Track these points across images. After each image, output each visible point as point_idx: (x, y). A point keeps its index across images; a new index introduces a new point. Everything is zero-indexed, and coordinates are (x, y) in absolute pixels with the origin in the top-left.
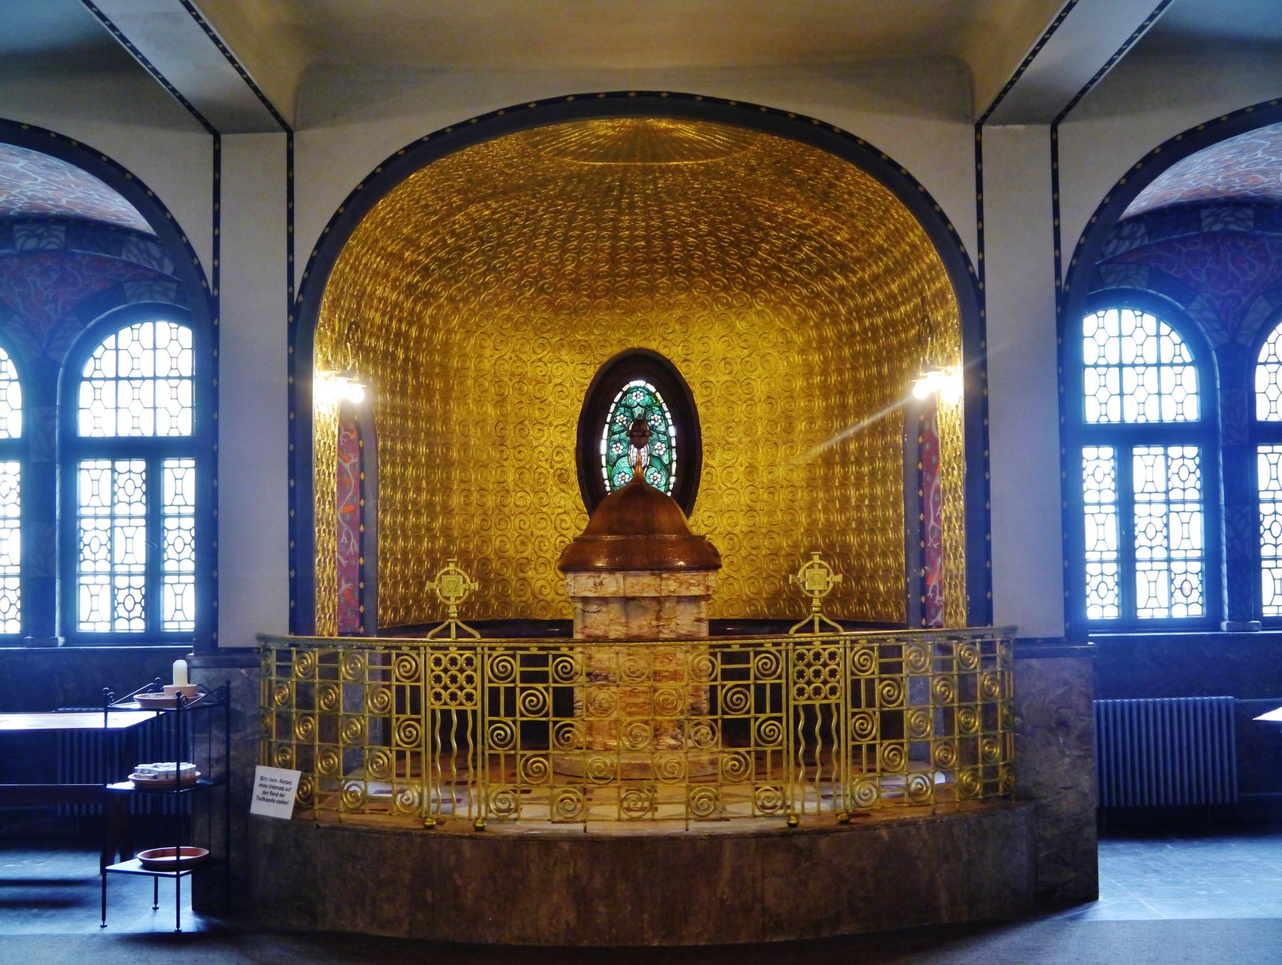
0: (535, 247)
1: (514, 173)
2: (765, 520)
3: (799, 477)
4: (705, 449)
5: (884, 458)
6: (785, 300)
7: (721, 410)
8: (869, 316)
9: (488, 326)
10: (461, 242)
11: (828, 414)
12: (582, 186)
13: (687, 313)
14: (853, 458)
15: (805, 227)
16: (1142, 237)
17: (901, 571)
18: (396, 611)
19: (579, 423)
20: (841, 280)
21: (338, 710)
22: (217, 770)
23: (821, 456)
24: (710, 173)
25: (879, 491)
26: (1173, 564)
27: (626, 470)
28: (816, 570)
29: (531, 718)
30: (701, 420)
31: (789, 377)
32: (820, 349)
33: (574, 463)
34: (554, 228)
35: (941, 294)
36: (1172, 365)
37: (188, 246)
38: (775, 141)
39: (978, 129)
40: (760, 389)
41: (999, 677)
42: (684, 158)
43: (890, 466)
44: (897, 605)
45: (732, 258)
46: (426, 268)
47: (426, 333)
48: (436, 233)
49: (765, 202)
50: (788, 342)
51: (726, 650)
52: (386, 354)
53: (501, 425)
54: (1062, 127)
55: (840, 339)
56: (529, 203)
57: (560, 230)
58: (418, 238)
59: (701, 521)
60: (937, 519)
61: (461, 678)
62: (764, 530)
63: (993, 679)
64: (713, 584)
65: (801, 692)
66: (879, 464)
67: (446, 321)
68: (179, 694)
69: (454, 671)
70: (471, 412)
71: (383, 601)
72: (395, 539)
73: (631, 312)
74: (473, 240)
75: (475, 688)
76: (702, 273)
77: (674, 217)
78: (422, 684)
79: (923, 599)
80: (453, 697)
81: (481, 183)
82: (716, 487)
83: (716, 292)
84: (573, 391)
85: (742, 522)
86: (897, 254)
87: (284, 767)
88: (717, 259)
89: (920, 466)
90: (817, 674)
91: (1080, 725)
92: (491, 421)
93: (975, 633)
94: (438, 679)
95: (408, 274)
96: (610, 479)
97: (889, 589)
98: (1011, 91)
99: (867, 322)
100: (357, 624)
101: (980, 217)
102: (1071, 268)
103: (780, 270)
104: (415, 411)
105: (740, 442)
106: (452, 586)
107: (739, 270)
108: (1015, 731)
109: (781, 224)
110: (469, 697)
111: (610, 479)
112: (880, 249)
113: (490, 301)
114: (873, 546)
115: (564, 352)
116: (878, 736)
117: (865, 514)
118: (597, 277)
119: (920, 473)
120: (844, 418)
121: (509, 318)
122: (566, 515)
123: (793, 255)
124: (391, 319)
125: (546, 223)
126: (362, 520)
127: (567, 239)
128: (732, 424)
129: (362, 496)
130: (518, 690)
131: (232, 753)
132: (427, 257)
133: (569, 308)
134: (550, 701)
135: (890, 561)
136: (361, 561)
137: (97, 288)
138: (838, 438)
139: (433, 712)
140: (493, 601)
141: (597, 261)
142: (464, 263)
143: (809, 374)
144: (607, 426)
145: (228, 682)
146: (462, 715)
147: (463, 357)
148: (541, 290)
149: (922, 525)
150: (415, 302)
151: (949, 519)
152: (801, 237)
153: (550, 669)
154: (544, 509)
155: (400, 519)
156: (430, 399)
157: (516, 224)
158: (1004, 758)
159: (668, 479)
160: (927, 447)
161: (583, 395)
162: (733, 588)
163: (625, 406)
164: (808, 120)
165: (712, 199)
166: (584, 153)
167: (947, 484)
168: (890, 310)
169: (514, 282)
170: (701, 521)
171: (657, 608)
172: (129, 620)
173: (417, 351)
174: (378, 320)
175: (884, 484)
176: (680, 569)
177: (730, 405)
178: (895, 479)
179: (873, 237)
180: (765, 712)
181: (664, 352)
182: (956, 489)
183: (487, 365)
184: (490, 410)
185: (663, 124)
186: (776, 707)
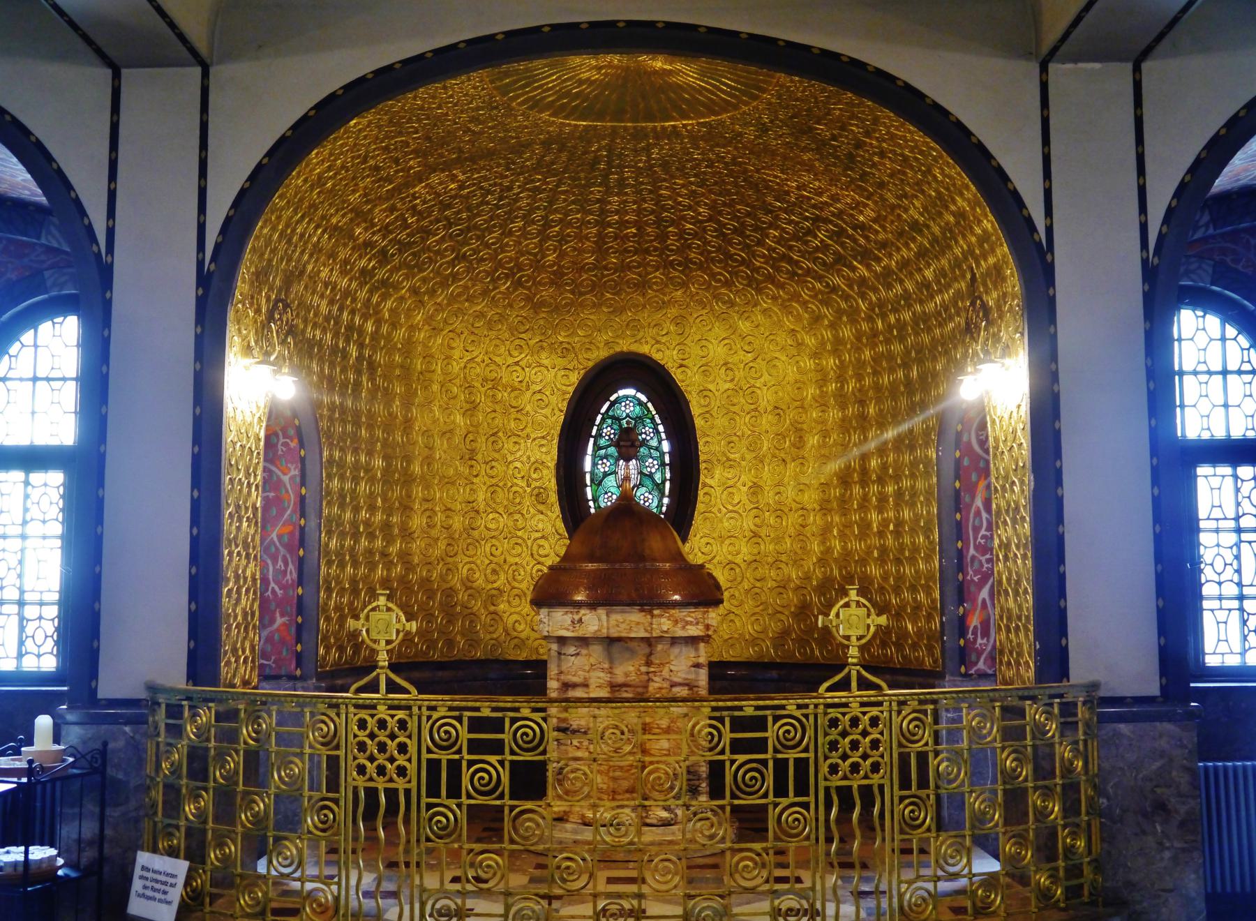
0: (511, 233)
1: (481, 133)
2: (771, 547)
3: (811, 498)
4: (702, 466)
5: (913, 476)
6: (796, 297)
7: (721, 422)
8: (895, 310)
9: (457, 324)
10: (425, 223)
11: (845, 426)
12: (564, 156)
13: (683, 312)
14: (874, 477)
15: (821, 207)
16: (1207, 225)
17: (935, 608)
18: (341, 649)
19: (561, 436)
20: (863, 271)
21: (237, 784)
22: (89, 855)
23: (836, 474)
24: (712, 136)
25: (906, 514)
26: (1245, 602)
27: (613, 490)
28: (853, 609)
29: (481, 800)
30: (698, 433)
31: (799, 385)
32: (836, 352)
33: (554, 481)
34: (532, 210)
35: (997, 271)
36: (1240, 372)
37: (78, 203)
38: (794, 83)
39: (1044, 68)
40: (766, 398)
41: (1081, 747)
42: (685, 116)
43: (920, 485)
44: (930, 649)
45: (735, 241)
46: (383, 252)
47: (385, 329)
48: (392, 209)
49: (774, 176)
50: (799, 344)
51: (737, 713)
52: (334, 350)
53: (471, 437)
54: (1145, 66)
55: (859, 339)
56: (503, 177)
57: (539, 213)
58: (370, 211)
59: (699, 547)
60: (985, 549)
61: (392, 746)
62: (770, 560)
63: (1075, 750)
64: (713, 623)
65: (834, 769)
66: (906, 483)
67: (408, 317)
68: (30, 762)
69: (382, 737)
70: (437, 418)
71: (325, 638)
72: (342, 565)
73: (620, 311)
74: (438, 221)
75: (409, 760)
76: (700, 267)
77: (670, 198)
78: (341, 753)
79: (962, 642)
80: (381, 771)
81: (443, 143)
82: (715, 510)
83: (716, 288)
84: (553, 399)
85: (744, 550)
86: (936, 230)
87: (170, 855)
88: (719, 249)
89: (957, 484)
90: (855, 745)
91: (1183, 809)
92: (460, 433)
93: (1053, 692)
94: (362, 747)
95: (360, 257)
96: (595, 500)
97: (919, 629)
98: (1073, 36)
99: (892, 319)
100: (293, 666)
101: (1047, 174)
102: (1161, 237)
103: (790, 261)
104: (371, 416)
105: (743, 459)
106: (381, 626)
107: (743, 262)
108: (1101, 817)
109: (794, 204)
110: (402, 771)
111: (595, 500)
112: (915, 226)
113: (459, 295)
114: (900, 578)
115: (544, 355)
116: (933, 827)
117: (890, 541)
118: (582, 269)
119: (957, 493)
120: (864, 430)
121: (481, 315)
122: (544, 537)
123: (806, 243)
124: (341, 309)
125: (523, 203)
126: (302, 543)
127: (547, 225)
128: (735, 438)
129: (303, 515)
130: (464, 764)
131: (108, 832)
132: (384, 238)
133: (550, 305)
134: (505, 779)
135: (921, 597)
136: (300, 591)
137: (13, 276)
138: (856, 452)
139: (355, 789)
140: (458, 638)
141: (581, 251)
142: (429, 249)
143: (822, 381)
144: (592, 440)
145: (105, 744)
146: (392, 794)
147: (428, 357)
148: (518, 284)
149: (961, 554)
150: (371, 292)
151: (1006, 546)
152: (817, 219)
153: (506, 737)
154: (520, 533)
155: (348, 542)
156: (388, 404)
157: (488, 203)
158: (1090, 852)
159: (660, 500)
160: (966, 462)
161: (565, 404)
162: (738, 626)
163: (613, 417)
164: (836, 56)
165: (714, 174)
166: (563, 107)
167: (1003, 504)
168: (921, 302)
169: (488, 274)
170: (699, 547)
171: (647, 650)
172: (39, 656)
173: (373, 349)
174: (324, 308)
175: (912, 505)
176: (675, 605)
177: (732, 416)
178: (927, 499)
179: (906, 210)
180: (787, 796)
181: (657, 356)
182: (1017, 509)
183: (456, 367)
184: (459, 419)
185: (659, 63)
186: (802, 789)
